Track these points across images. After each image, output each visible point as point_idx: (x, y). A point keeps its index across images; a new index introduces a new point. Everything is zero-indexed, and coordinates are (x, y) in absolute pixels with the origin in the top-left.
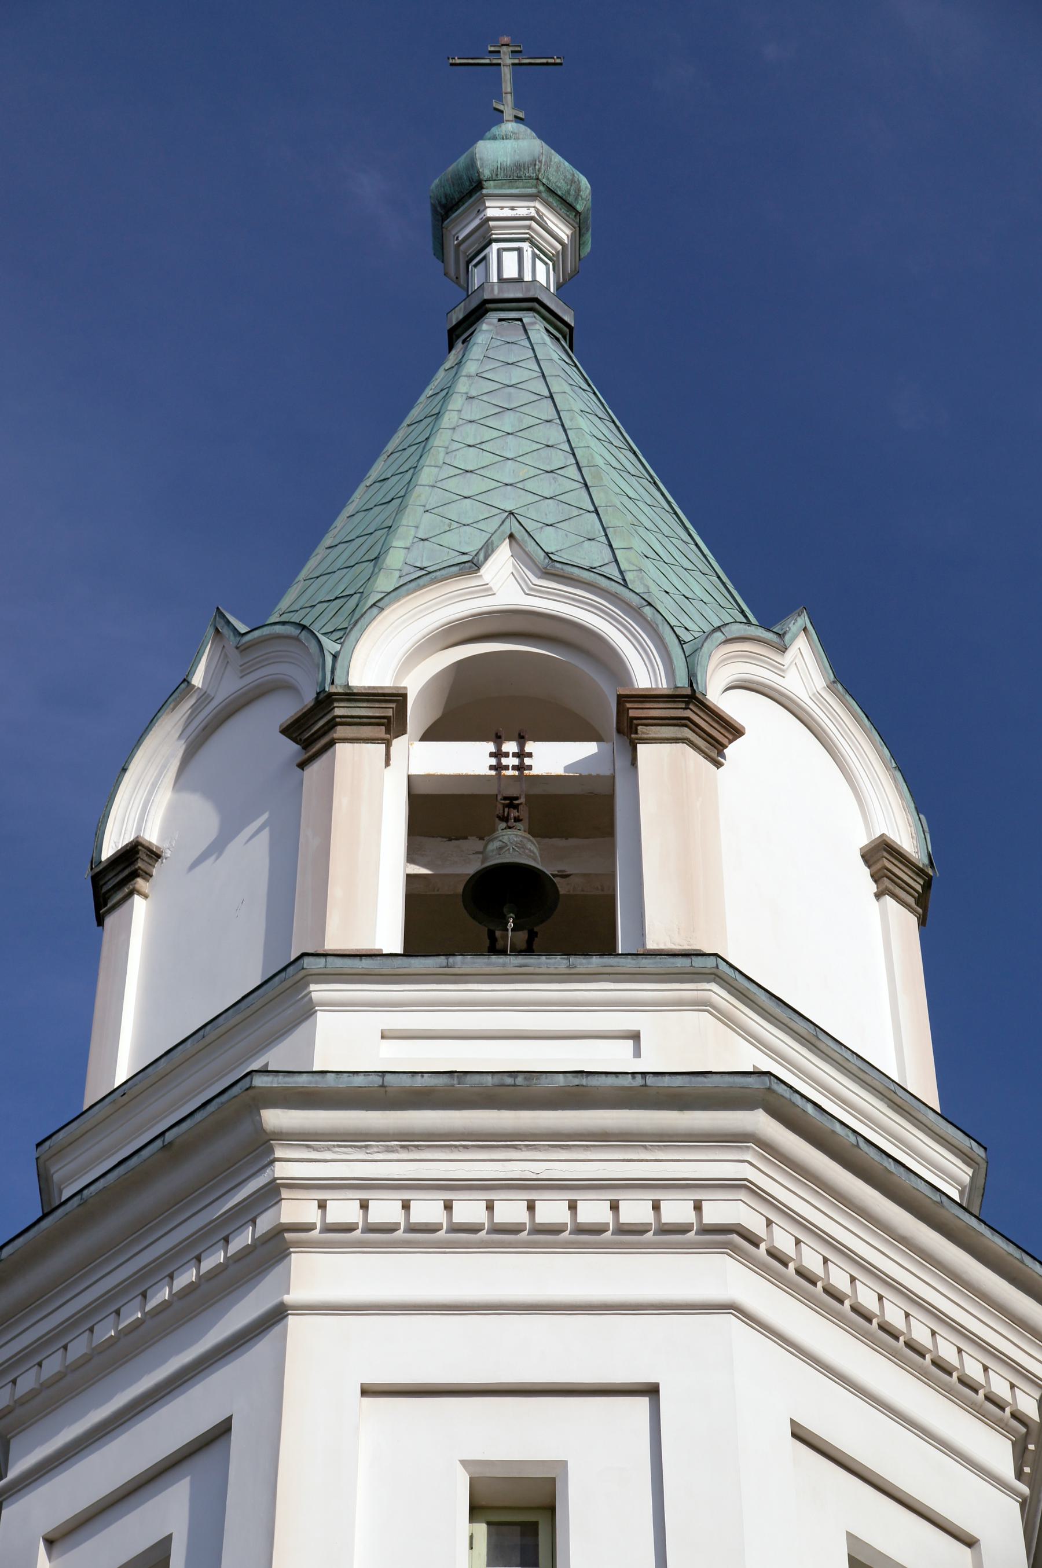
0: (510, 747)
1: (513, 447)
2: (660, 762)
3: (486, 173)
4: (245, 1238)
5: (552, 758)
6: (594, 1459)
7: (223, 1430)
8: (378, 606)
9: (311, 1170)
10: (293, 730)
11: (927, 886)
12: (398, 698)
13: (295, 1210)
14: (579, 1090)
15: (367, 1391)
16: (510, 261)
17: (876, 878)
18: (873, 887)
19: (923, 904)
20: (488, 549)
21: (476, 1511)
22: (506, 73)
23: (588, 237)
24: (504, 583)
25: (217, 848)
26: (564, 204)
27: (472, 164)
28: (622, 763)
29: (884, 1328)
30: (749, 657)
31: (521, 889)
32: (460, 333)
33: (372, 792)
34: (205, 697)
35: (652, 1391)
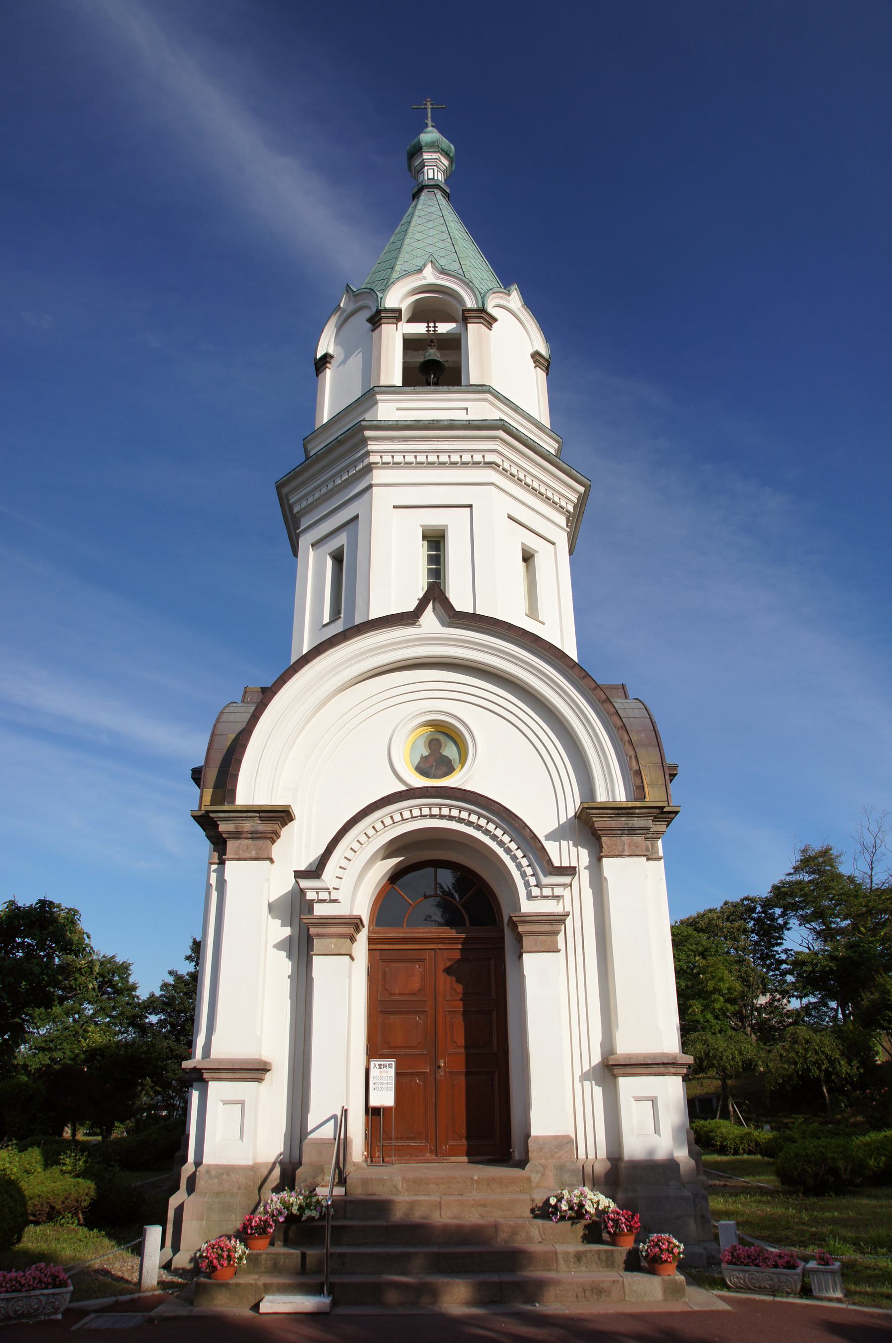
0: (432, 325)
2: (474, 330)
3: (423, 144)
5: (444, 328)
9: (378, 448)
11: (549, 364)
13: (374, 458)
14: (451, 425)
15: (394, 507)
16: (431, 172)
17: (535, 362)
19: (547, 370)
20: (425, 265)
21: (424, 537)
22: (429, 111)
24: (430, 276)
25: (344, 362)
26: (446, 154)
27: (419, 141)
28: (463, 329)
31: (436, 366)
32: (416, 195)
33: (392, 340)
35: (470, 506)
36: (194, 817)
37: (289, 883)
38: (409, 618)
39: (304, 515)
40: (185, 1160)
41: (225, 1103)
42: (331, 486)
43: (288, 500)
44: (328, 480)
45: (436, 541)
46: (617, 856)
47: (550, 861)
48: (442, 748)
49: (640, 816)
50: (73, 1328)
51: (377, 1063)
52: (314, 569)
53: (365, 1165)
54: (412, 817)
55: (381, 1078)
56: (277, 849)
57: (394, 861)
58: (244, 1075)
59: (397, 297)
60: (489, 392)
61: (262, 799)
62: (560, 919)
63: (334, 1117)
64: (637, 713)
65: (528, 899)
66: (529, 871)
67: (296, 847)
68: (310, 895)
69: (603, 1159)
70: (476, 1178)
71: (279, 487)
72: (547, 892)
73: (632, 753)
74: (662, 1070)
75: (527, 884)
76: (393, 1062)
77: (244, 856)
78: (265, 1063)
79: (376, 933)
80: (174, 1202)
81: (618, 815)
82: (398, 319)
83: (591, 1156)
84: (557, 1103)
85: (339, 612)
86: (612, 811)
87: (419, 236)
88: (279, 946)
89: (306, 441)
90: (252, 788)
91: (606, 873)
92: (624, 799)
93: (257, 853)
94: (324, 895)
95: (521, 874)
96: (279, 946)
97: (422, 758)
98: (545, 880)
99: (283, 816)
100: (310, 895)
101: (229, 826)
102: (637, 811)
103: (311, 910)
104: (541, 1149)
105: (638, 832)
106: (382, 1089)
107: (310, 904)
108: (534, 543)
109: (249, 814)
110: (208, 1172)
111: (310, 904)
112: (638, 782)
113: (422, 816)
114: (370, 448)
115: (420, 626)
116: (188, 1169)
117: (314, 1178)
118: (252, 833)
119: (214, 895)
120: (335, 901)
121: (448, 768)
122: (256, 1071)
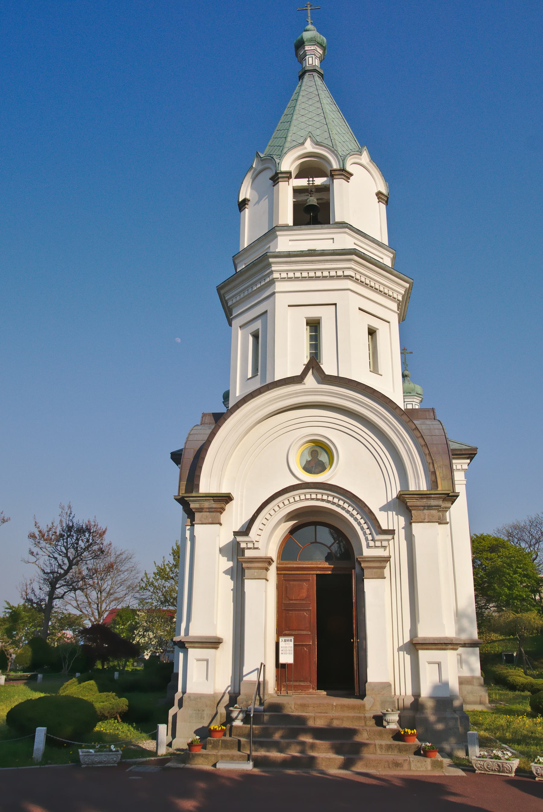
0: (311, 179)
1: (312, 109)
2: (338, 184)
3: (305, 40)
4: (268, 280)
5: (319, 181)
6: (326, 316)
7: (266, 312)
8: (286, 153)
9: (278, 268)
10: (271, 179)
11: (388, 199)
12: (290, 173)
13: (276, 275)
14: (323, 253)
15: (289, 306)
16: (310, 59)
17: (378, 199)
18: (378, 200)
19: (387, 203)
20: (306, 140)
21: (307, 324)
22: (309, 11)
23: (326, 51)
24: (309, 147)
25: (258, 202)
26: (321, 45)
27: (302, 38)
28: (331, 182)
29: (375, 288)
30: (355, 158)
31: (314, 211)
32: (301, 77)
33: (286, 195)
34: (255, 169)
35: (335, 304)
36: (176, 499)
37: (231, 537)
38: (298, 379)
39: (235, 307)
40: (176, 690)
41: (198, 660)
42: (250, 290)
43: (225, 298)
44: (248, 287)
45: (314, 325)
46: (421, 522)
47: (380, 526)
48: (319, 456)
49: (434, 499)
50: (127, 770)
51: (283, 639)
52: (241, 342)
53: (276, 695)
54: (300, 500)
55: (286, 647)
56: (224, 517)
57: (291, 523)
58: (208, 645)
59: (289, 163)
60: (347, 227)
61: (214, 490)
62: (387, 559)
63: (257, 669)
64: (437, 432)
65: (367, 548)
66: (368, 532)
67: (234, 516)
68: (243, 545)
69: (409, 696)
70: (335, 704)
71: (219, 289)
72: (378, 544)
73: (430, 461)
74: (444, 647)
75: (367, 539)
76: (292, 638)
77: (205, 522)
78: (219, 639)
79: (281, 564)
80: (171, 712)
81: (421, 498)
82: (290, 177)
83: (403, 693)
84: (383, 663)
85: (257, 370)
86: (418, 496)
87: (303, 112)
88: (226, 572)
89: (235, 258)
90: (207, 484)
91: (414, 532)
92: (425, 489)
93: (212, 520)
94: (250, 545)
95: (363, 533)
96: (226, 572)
97: (307, 461)
98: (377, 537)
99: (227, 498)
100: (243, 545)
101: (196, 506)
102: (433, 496)
103: (243, 554)
104: (373, 689)
105: (433, 508)
106: (286, 654)
107: (243, 550)
108: (375, 323)
109: (207, 498)
110: (189, 697)
111: (243, 550)
112: (433, 478)
113: (306, 499)
114: (273, 269)
115: (304, 384)
116: (178, 696)
117: (247, 702)
118: (209, 508)
119: (189, 543)
120: (257, 548)
121: (320, 468)
122: (214, 643)
